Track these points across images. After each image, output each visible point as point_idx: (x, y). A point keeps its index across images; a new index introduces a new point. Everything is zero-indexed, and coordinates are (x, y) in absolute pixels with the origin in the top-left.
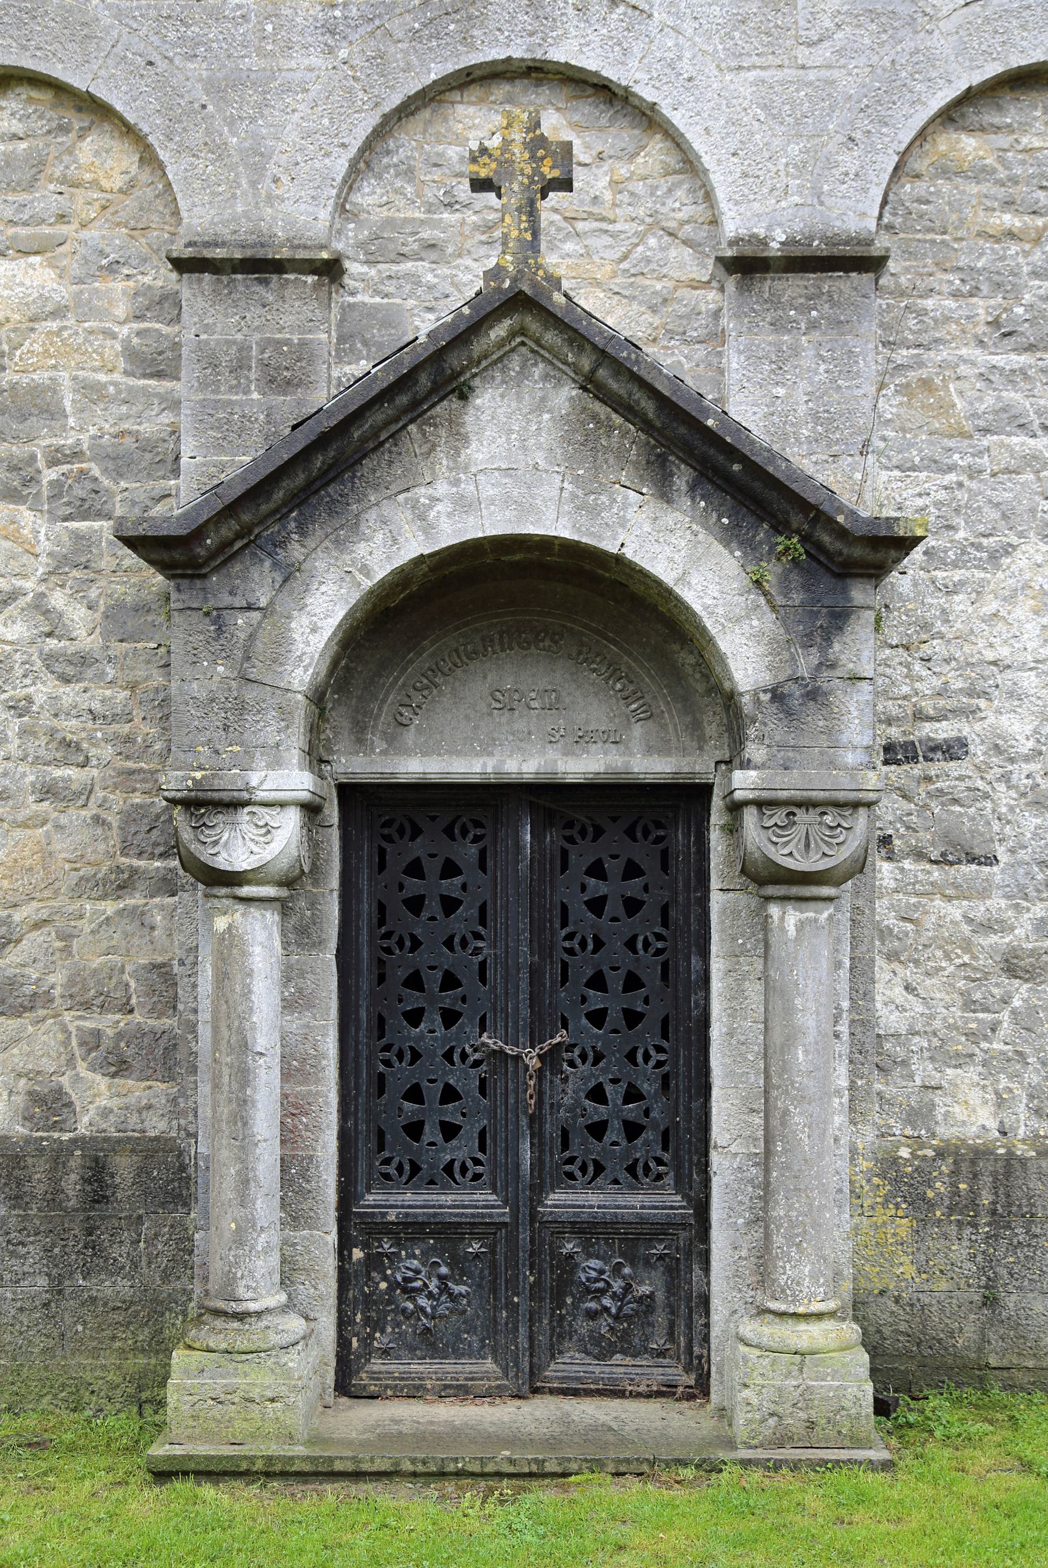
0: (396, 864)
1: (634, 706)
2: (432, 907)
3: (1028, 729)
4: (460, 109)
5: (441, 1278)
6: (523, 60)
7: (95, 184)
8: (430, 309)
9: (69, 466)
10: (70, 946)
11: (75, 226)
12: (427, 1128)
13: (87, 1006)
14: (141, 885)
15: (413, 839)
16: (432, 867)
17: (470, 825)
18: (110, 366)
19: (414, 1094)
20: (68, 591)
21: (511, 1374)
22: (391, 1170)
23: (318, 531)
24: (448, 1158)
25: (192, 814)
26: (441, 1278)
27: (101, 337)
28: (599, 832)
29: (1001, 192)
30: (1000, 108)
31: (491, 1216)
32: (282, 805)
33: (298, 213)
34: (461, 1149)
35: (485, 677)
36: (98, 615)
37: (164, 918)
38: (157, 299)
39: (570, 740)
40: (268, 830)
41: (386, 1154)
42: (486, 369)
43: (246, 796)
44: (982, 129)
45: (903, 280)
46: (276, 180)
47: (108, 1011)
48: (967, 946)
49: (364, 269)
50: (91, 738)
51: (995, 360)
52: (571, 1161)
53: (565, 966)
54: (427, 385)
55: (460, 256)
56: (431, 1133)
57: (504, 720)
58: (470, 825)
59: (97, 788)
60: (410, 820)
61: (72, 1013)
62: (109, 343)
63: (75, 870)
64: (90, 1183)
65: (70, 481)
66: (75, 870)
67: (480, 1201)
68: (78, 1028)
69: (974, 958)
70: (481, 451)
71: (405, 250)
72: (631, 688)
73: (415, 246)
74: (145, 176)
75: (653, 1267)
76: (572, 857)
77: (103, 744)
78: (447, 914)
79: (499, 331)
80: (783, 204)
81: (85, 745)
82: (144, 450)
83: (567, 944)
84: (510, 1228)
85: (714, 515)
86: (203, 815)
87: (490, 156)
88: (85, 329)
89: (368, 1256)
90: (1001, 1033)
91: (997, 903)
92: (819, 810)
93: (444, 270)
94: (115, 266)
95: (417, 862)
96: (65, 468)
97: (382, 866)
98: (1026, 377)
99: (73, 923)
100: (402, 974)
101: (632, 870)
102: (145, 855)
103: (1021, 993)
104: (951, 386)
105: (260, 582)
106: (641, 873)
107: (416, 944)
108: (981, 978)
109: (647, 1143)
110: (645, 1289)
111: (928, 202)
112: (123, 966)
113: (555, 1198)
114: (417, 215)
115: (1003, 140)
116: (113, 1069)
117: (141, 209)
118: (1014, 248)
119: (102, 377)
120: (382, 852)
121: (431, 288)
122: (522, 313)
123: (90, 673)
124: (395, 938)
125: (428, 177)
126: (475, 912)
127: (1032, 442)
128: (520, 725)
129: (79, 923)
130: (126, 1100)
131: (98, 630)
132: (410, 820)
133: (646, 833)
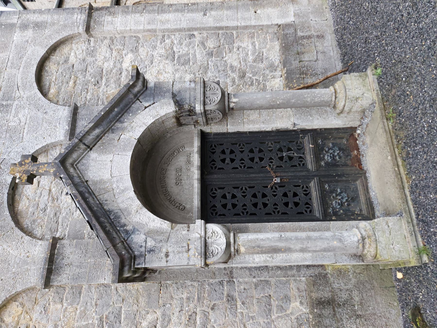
0: (224, 211)
1: (181, 150)
2: (235, 201)
3: (188, 75)
4: (19, 208)
5: (337, 195)
6: (9, 190)
7: (19, 317)
8: (73, 214)
9: (104, 322)
10: (252, 316)
11: (31, 323)
12: (295, 201)
13: (270, 310)
14: (232, 293)
15: (216, 207)
16: (224, 201)
17: (212, 192)
18: (75, 309)
19: (286, 204)
20: (142, 321)
21: (360, 175)
22: (308, 210)
23: (123, 221)
24: (303, 195)
25: (208, 257)
26: (337, 195)
27: (66, 313)
28: (213, 161)
29: (64, 84)
30: (45, 85)
31: (317, 182)
32: (205, 228)
33: (39, 250)
34: (299, 191)
35: (172, 187)
36: (151, 310)
37: (241, 285)
38: (57, 294)
39: (189, 165)
40: (213, 232)
41: (304, 212)
42: (82, 175)
43: (203, 239)
44: (49, 88)
45: (82, 103)
46: (28, 257)
47: (270, 303)
48: (238, 86)
49: (59, 232)
50: (188, 312)
51: (103, 84)
52: (299, 165)
53: (248, 168)
54: (87, 196)
55: (59, 207)
56: (296, 199)
57: (184, 182)
58: (212, 192)
59: (203, 309)
60: (210, 208)
61: (272, 315)
62: (68, 310)
63: (228, 316)
64: (325, 306)
65: (109, 322)
66: (228, 316)
67: (313, 185)
68: (277, 313)
69: (241, 84)
70: (106, 176)
71: (55, 221)
72: (176, 151)
73: (55, 218)
74: (20, 300)
75: (325, 143)
76: (220, 167)
77: (190, 307)
78: (236, 197)
79: (72, 170)
80: (58, 127)
81: (190, 313)
82: (102, 297)
83: (243, 167)
84: (320, 177)
85: (129, 117)
86: (209, 254)
87: (21, 176)
88: (63, 318)
89: (334, 215)
90: (258, 78)
91: (228, 81)
92: (206, 92)
93: (63, 211)
94: (45, 309)
95: (222, 205)
96: (104, 323)
97: (224, 215)
98: (108, 78)
99: (244, 316)
100: (253, 208)
101: (223, 152)
102: (223, 292)
103: (249, 75)
104: (108, 93)
105: (138, 239)
106: (224, 150)
107: (245, 205)
108: (245, 83)
109: (292, 146)
110: (331, 145)
111: (64, 99)
112: (257, 299)
113: (310, 167)
114: (46, 219)
115: (53, 84)
116: (288, 301)
117: (30, 301)
118: (78, 82)
119: (78, 312)
120: (220, 215)
121: (67, 214)
122: (67, 165)
123: (168, 312)
124: (244, 211)
125: (36, 216)
126: (235, 190)
127: (123, 77)
128: (185, 178)
129: (244, 314)
130: (297, 297)
131: (155, 310)
132: (210, 208)
133: (213, 149)
